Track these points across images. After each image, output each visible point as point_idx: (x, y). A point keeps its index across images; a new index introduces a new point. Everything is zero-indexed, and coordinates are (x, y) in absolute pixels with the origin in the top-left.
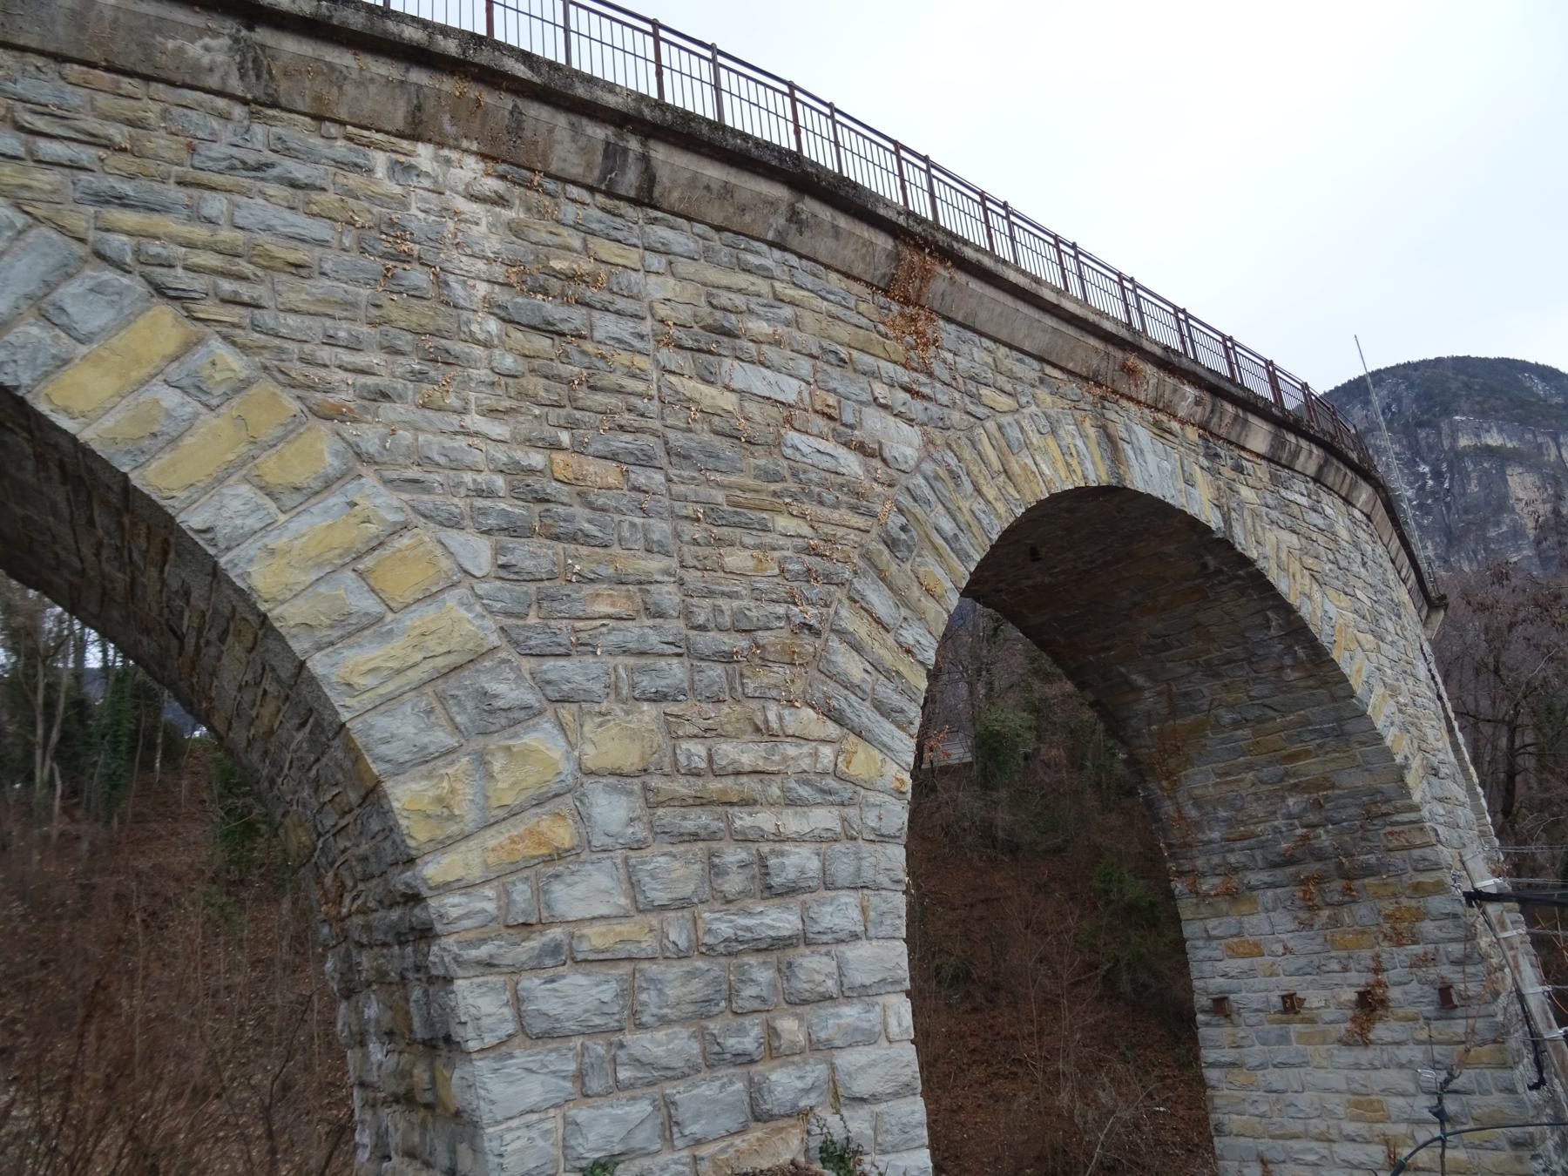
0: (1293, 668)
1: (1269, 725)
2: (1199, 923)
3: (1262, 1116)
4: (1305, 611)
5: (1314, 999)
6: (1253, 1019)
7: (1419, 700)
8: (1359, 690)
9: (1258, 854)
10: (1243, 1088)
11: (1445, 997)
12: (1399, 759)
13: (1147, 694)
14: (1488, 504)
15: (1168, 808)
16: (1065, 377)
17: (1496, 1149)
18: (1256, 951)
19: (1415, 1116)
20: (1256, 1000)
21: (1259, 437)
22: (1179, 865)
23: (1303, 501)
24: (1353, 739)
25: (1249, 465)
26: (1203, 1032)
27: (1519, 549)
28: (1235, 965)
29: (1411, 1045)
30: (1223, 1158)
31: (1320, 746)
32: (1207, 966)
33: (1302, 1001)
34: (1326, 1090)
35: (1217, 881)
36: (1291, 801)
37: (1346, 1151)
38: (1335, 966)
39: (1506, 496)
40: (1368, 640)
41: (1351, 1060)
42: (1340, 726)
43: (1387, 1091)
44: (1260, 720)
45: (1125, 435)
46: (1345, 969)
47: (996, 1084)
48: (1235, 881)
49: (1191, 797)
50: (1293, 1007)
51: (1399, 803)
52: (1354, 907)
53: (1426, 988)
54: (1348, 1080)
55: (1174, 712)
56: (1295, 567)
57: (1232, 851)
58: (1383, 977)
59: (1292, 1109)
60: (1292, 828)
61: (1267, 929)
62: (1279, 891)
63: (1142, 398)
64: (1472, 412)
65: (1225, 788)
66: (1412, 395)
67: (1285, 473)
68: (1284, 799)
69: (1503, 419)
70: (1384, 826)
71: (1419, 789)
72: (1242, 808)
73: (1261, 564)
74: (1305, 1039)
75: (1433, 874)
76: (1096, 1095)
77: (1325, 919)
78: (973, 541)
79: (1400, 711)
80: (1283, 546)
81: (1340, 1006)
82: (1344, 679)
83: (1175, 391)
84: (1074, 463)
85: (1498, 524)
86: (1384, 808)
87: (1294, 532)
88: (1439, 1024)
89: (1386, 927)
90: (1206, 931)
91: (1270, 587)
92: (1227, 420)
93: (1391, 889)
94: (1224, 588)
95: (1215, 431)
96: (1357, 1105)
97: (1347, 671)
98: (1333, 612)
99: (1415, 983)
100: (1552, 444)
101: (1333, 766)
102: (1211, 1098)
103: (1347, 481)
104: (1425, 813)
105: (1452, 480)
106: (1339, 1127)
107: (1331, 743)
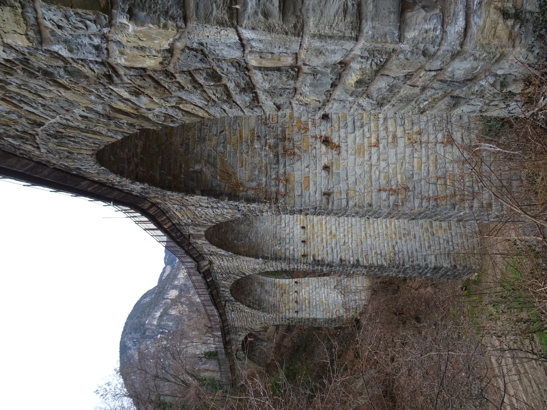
2: (296, 197)
5: (325, 161)
6: (331, 185)
13: (204, 170)
18: (307, 178)
19: (362, 136)
20: (324, 182)
22: (273, 198)
28: (312, 188)
31: (239, 126)
32: (312, 199)
35: (281, 185)
36: (256, 146)
37: (374, 158)
38: (314, 151)
41: (345, 152)
43: (355, 141)
46: (315, 148)
49: (248, 181)
52: (295, 140)
57: (271, 176)
61: (300, 172)
62: (287, 164)
65: (247, 166)
66: (133, 334)
68: (255, 148)
74: (338, 168)
81: (327, 152)
89: (302, 131)
90: (299, 196)
96: (359, 153)
101: (247, 125)
105: (166, 329)
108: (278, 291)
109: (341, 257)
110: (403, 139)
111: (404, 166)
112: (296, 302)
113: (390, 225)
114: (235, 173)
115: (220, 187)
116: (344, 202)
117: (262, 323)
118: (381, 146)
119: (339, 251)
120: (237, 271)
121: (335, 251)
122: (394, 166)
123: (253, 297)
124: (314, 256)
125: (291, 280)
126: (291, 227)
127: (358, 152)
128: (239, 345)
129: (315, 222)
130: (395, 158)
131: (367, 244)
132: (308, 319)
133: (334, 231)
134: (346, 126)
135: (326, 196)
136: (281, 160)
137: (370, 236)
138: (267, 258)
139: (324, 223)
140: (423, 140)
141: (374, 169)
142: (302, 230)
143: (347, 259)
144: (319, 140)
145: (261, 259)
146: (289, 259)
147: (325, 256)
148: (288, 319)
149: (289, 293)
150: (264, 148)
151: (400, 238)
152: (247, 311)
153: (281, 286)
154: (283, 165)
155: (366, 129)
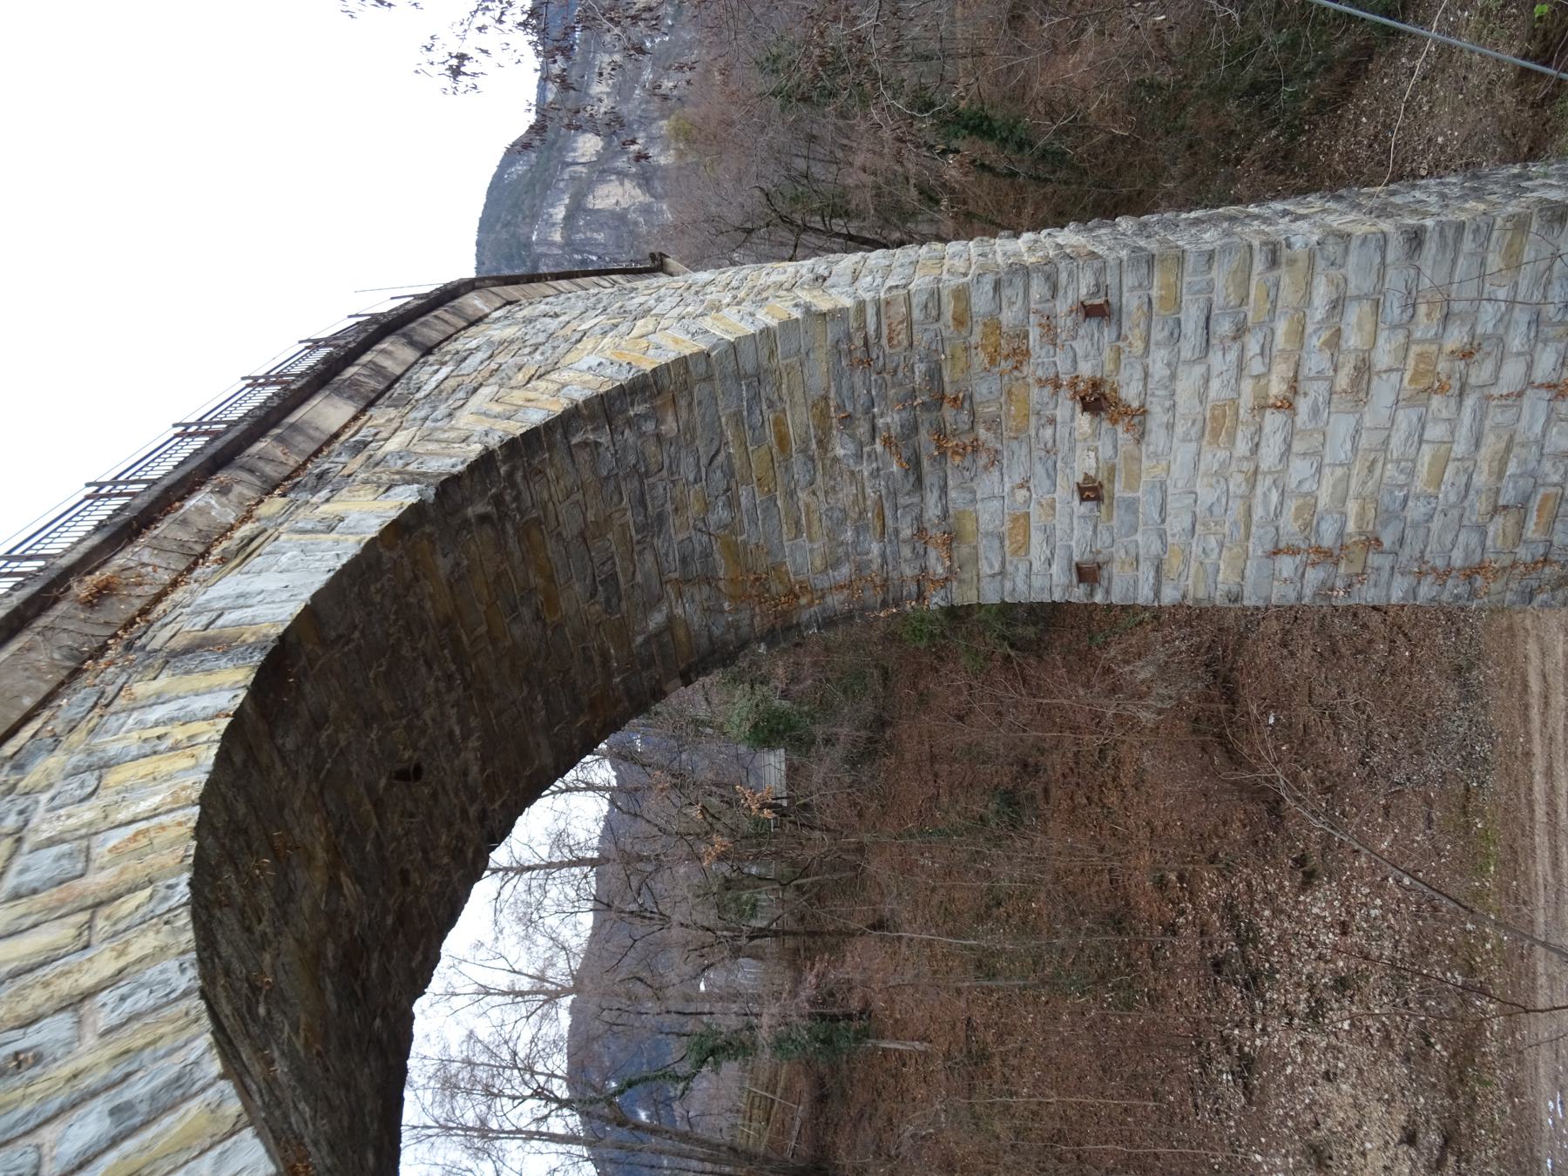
0: (658, 423)
1: (737, 464)
2: (985, 583)
3: (1221, 545)
4: (579, 394)
5: (1085, 464)
7: (734, 284)
8: (702, 345)
9: (903, 500)
10: (1186, 563)
11: (1097, 312)
12: (797, 314)
13: (679, 611)
14: (616, 228)
15: (836, 601)
16: (46, 714)
17: (1277, 285)
19: (1233, 372)
21: (329, 412)
22: (909, 597)
23: (445, 371)
24: (765, 363)
25: (364, 432)
26: (1116, 599)
29: (1149, 361)
30: (1268, 598)
31: (771, 405)
32: (1037, 582)
33: (1087, 477)
34: (1196, 467)
35: (933, 554)
36: (840, 452)
37: (1269, 455)
38: (1049, 432)
39: (612, 213)
40: (642, 326)
41: (1163, 432)
42: (746, 376)
43: (1202, 396)
44: (729, 473)
45: (204, 619)
46: (1052, 421)
47: (1124, 781)
48: (935, 533)
49: (824, 571)
50: (1094, 489)
51: (853, 324)
52: (977, 398)
53: (1082, 332)
54: (1186, 439)
55: (709, 579)
56: (518, 397)
57: (897, 532)
58: (1065, 379)
59: (1216, 510)
60: (873, 456)
61: (996, 504)
62: (950, 483)
63: (166, 577)
64: (531, 225)
67: (398, 388)
68: (836, 460)
69: (542, 202)
70: (880, 347)
71: (839, 298)
72: (844, 511)
73: (494, 442)
74: (1133, 481)
75: (945, 299)
76: (1143, 682)
77: (990, 435)
78: (163, 1046)
79: (739, 304)
80: (486, 407)
81: (1096, 434)
82: (683, 362)
83: (184, 522)
84: (179, 733)
85: (636, 223)
86: (858, 342)
87: (475, 390)
88: (1126, 325)
90: (993, 576)
91: (533, 437)
92: (278, 452)
93: (959, 353)
94: (526, 495)
95: (287, 471)
96: (1216, 434)
97: (672, 356)
98: (593, 360)
99: (1074, 344)
100: (572, 168)
101: (798, 394)
102: (1196, 600)
103: (447, 316)
104: (868, 296)
105: (590, 253)
106: (1240, 459)
107: (767, 391)
110: (1395, 377)
111: (1377, 472)
114: (776, 567)
115: (738, 628)
118: (1303, 405)
122: (1339, 472)
127: (1213, 429)
130: (1348, 446)
134: (1175, 336)
136: (931, 477)
140: (1473, 380)
141: (1263, 484)
144: (1070, 393)
150: (866, 449)
154: (936, 494)
155: (1253, 346)
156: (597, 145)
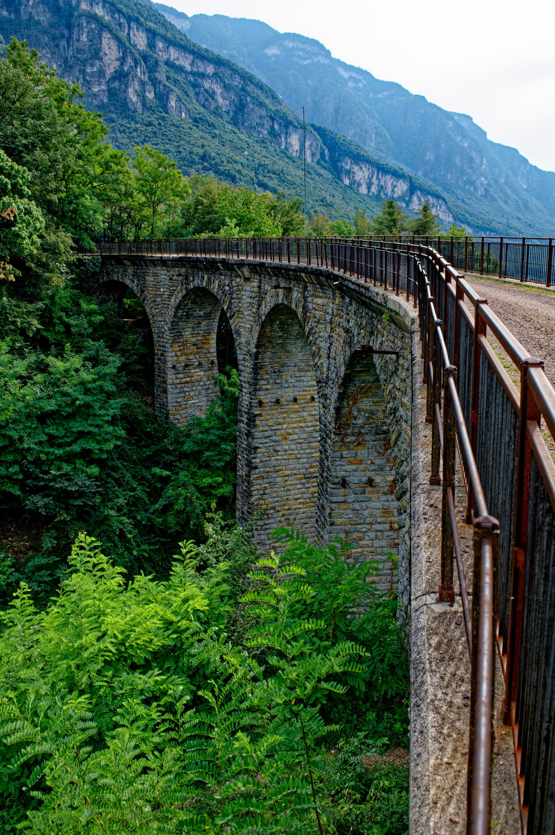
5: (378, 479)
10: (344, 509)
27: (100, 84)
28: (349, 468)
37: (378, 527)
41: (386, 499)
81: (387, 481)
85: (92, 65)
90: (342, 455)
96: (384, 513)
100: (126, 25)
108: (200, 338)
109: (260, 448)
112: (187, 366)
113: (299, 503)
114: (367, 397)
116: (335, 499)
117: (153, 316)
118: (390, 533)
119: (267, 445)
120: (235, 310)
121: (267, 440)
123: (192, 308)
124: (260, 415)
125: (215, 354)
126: (296, 384)
128: (118, 277)
129: (302, 414)
131: (276, 477)
132: (165, 382)
133: (291, 437)
135: (341, 481)
137: (286, 480)
138: (257, 358)
139: (301, 425)
141: (368, 527)
142: (291, 399)
143: (258, 455)
145: (254, 350)
146: (256, 385)
147: (261, 429)
148: (162, 355)
149: (197, 353)
151: (283, 515)
152: (172, 300)
153: (205, 341)
156: (140, 46)
